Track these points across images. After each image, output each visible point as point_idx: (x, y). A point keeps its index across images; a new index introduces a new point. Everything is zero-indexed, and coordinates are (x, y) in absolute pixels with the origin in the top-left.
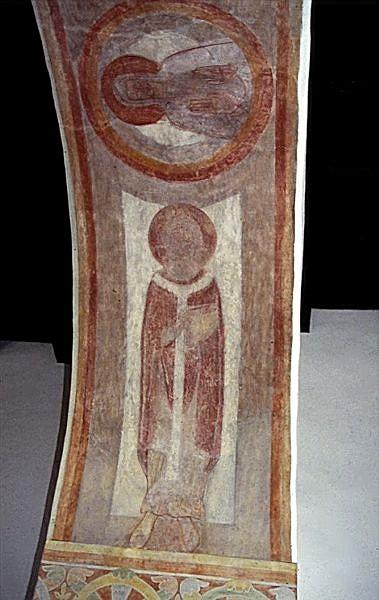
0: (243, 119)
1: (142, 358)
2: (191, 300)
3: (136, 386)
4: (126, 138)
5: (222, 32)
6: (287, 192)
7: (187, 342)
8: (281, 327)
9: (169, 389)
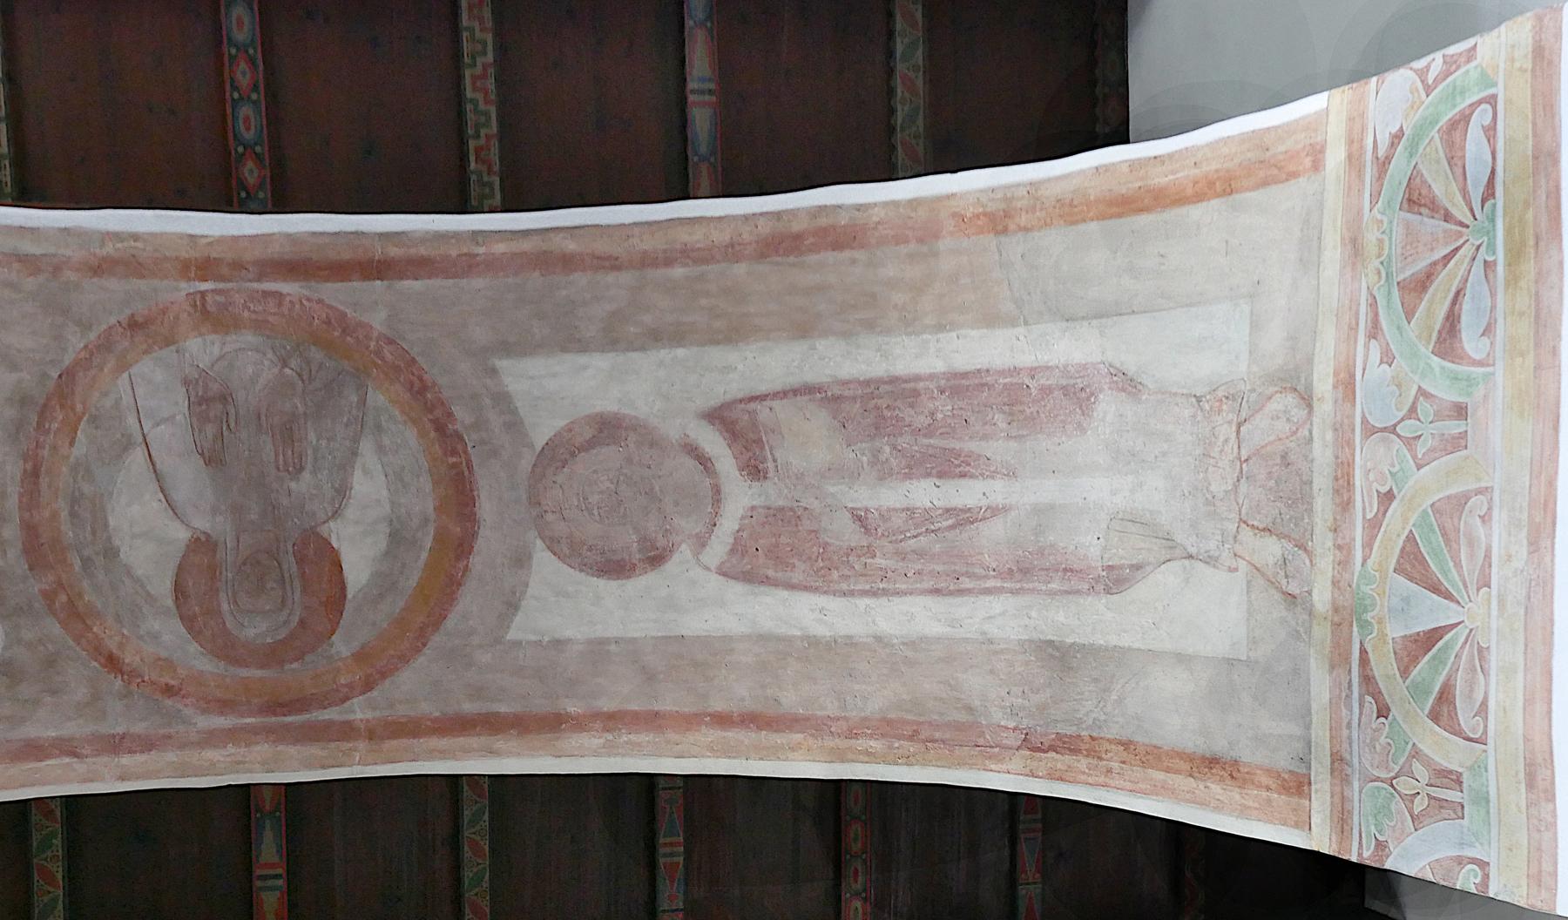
0: (316, 354)
1: (898, 593)
2: (754, 470)
5: (106, 394)
6: (481, 250)
7: (852, 475)
8: (798, 237)
9: (964, 518)
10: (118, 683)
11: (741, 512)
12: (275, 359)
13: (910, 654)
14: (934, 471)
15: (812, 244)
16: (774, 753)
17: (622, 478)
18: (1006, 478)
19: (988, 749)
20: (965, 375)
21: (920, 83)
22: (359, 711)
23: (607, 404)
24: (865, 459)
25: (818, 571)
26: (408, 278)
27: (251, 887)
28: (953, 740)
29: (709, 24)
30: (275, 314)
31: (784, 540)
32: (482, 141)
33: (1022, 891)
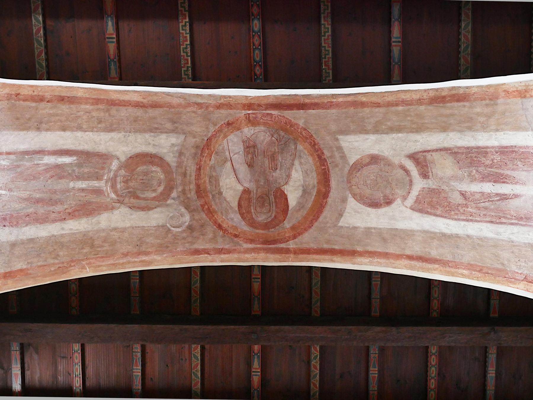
0: (282, 133)
1: (476, 221)
2: (425, 175)
3: (501, 228)
4: (300, 216)
5: (220, 145)
8: (444, 97)
9: (504, 197)
10: (221, 233)
11: (419, 189)
12: (269, 134)
13: (479, 242)
14: (492, 180)
15: (449, 100)
16: (428, 270)
17: (378, 176)
18: (521, 185)
19: (510, 279)
20: (506, 147)
21: (470, 37)
22: (291, 245)
23: (375, 152)
24: (466, 174)
25: (447, 211)
26: (311, 109)
27: (251, 281)
28: (496, 274)
29: (399, 20)
30: (270, 121)
31: (434, 199)
32: (327, 60)
33: (492, 302)
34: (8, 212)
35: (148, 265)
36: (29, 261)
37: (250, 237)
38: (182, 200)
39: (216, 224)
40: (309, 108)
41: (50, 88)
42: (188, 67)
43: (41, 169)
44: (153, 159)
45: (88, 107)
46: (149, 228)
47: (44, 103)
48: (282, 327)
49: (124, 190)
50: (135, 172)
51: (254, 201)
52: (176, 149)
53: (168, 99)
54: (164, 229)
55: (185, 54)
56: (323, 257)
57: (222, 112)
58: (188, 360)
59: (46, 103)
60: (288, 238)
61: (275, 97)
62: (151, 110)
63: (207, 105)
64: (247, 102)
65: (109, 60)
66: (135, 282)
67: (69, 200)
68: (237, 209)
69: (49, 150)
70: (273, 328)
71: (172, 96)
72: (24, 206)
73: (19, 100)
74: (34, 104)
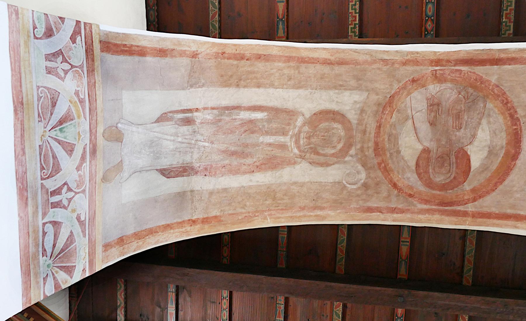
0: (471, 90)
5: (403, 103)
12: (456, 92)
22: (470, 208)
26: (506, 65)
30: (458, 77)
32: (508, 11)
34: (209, 163)
35: (322, 220)
36: (222, 209)
37: (426, 198)
38: (360, 158)
39: (392, 182)
40: (504, 64)
41: (250, 46)
42: (355, 24)
43: (237, 123)
44: (335, 116)
45: (280, 64)
46: (326, 183)
47: (244, 61)
48: (431, 293)
49: (306, 145)
50: (317, 129)
51: (433, 161)
52: (358, 106)
53: (355, 56)
54: (340, 185)
55: (353, 11)
56: (505, 222)
57: (408, 69)
58: (329, 317)
59: (246, 61)
60: (466, 201)
61: (467, 52)
62: (337, 67)
63: (393, 61)
64: (435, 58)
65: (278, 20)
66: (283, 236)
67: (258, 154)
68: (414, 168)
69: (245, 105)
70: (421, 293)
71: (359, 53)
72: (222, 158)
73: (224, 58)
74: (235, 62)
